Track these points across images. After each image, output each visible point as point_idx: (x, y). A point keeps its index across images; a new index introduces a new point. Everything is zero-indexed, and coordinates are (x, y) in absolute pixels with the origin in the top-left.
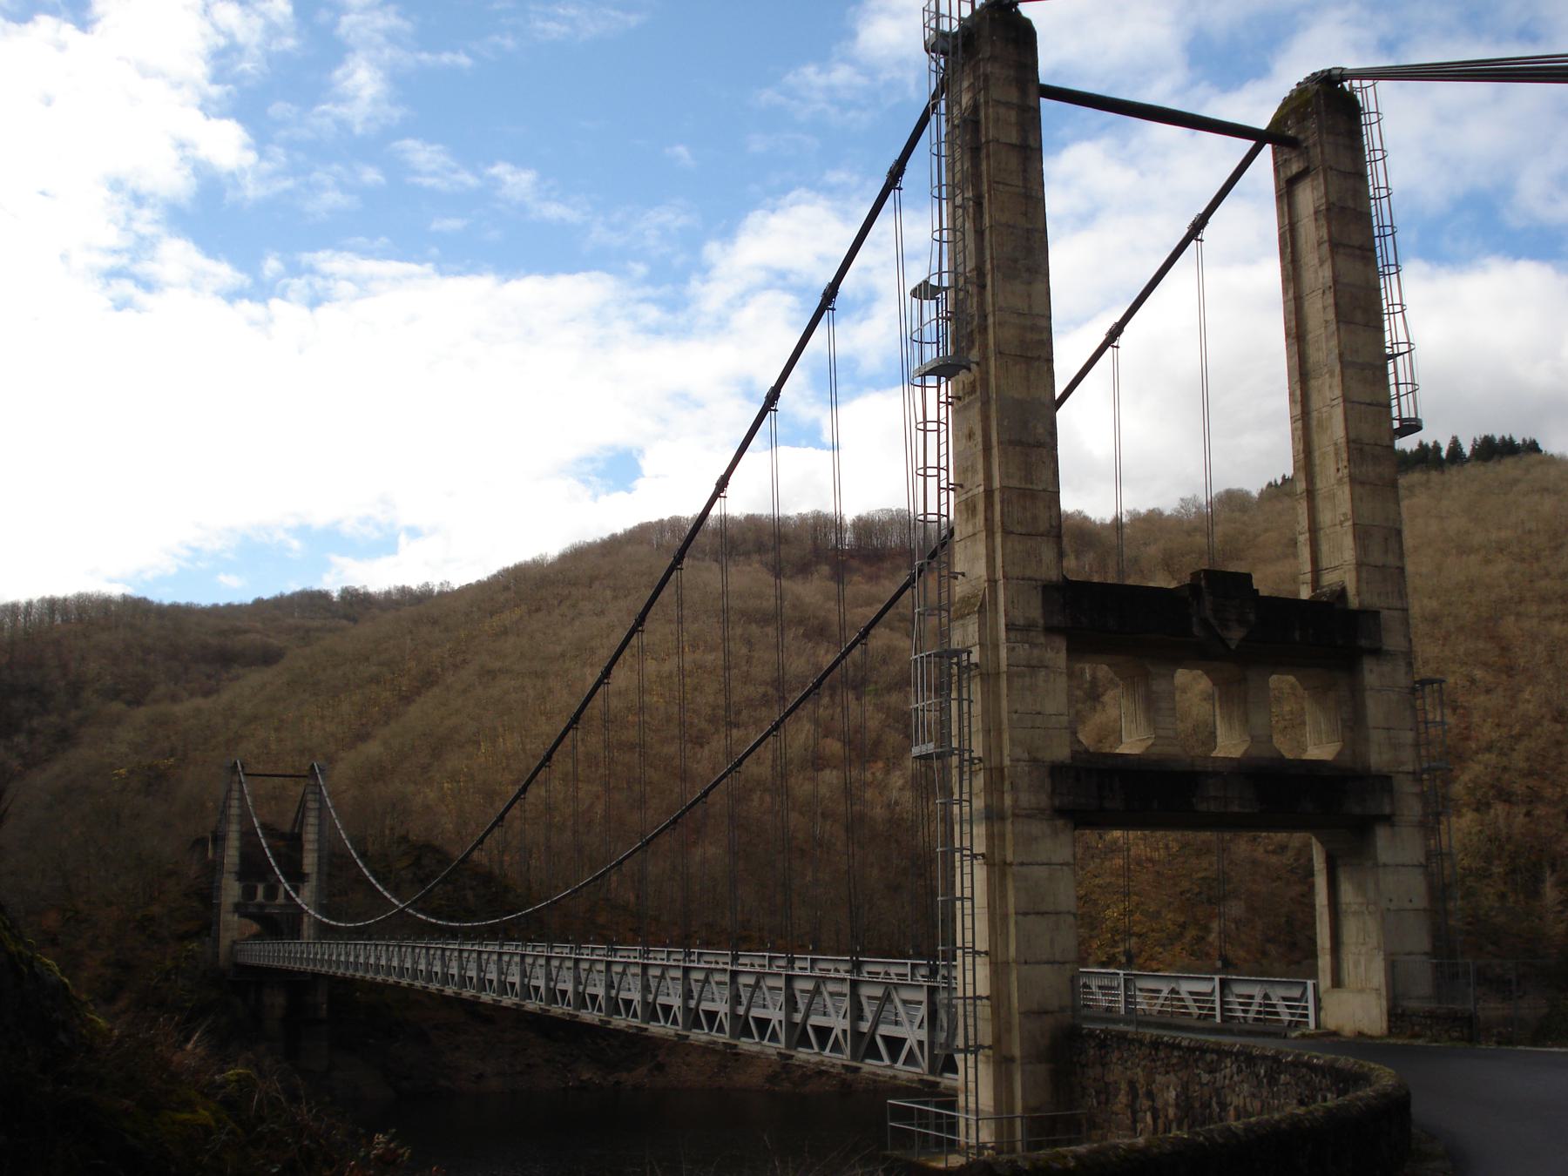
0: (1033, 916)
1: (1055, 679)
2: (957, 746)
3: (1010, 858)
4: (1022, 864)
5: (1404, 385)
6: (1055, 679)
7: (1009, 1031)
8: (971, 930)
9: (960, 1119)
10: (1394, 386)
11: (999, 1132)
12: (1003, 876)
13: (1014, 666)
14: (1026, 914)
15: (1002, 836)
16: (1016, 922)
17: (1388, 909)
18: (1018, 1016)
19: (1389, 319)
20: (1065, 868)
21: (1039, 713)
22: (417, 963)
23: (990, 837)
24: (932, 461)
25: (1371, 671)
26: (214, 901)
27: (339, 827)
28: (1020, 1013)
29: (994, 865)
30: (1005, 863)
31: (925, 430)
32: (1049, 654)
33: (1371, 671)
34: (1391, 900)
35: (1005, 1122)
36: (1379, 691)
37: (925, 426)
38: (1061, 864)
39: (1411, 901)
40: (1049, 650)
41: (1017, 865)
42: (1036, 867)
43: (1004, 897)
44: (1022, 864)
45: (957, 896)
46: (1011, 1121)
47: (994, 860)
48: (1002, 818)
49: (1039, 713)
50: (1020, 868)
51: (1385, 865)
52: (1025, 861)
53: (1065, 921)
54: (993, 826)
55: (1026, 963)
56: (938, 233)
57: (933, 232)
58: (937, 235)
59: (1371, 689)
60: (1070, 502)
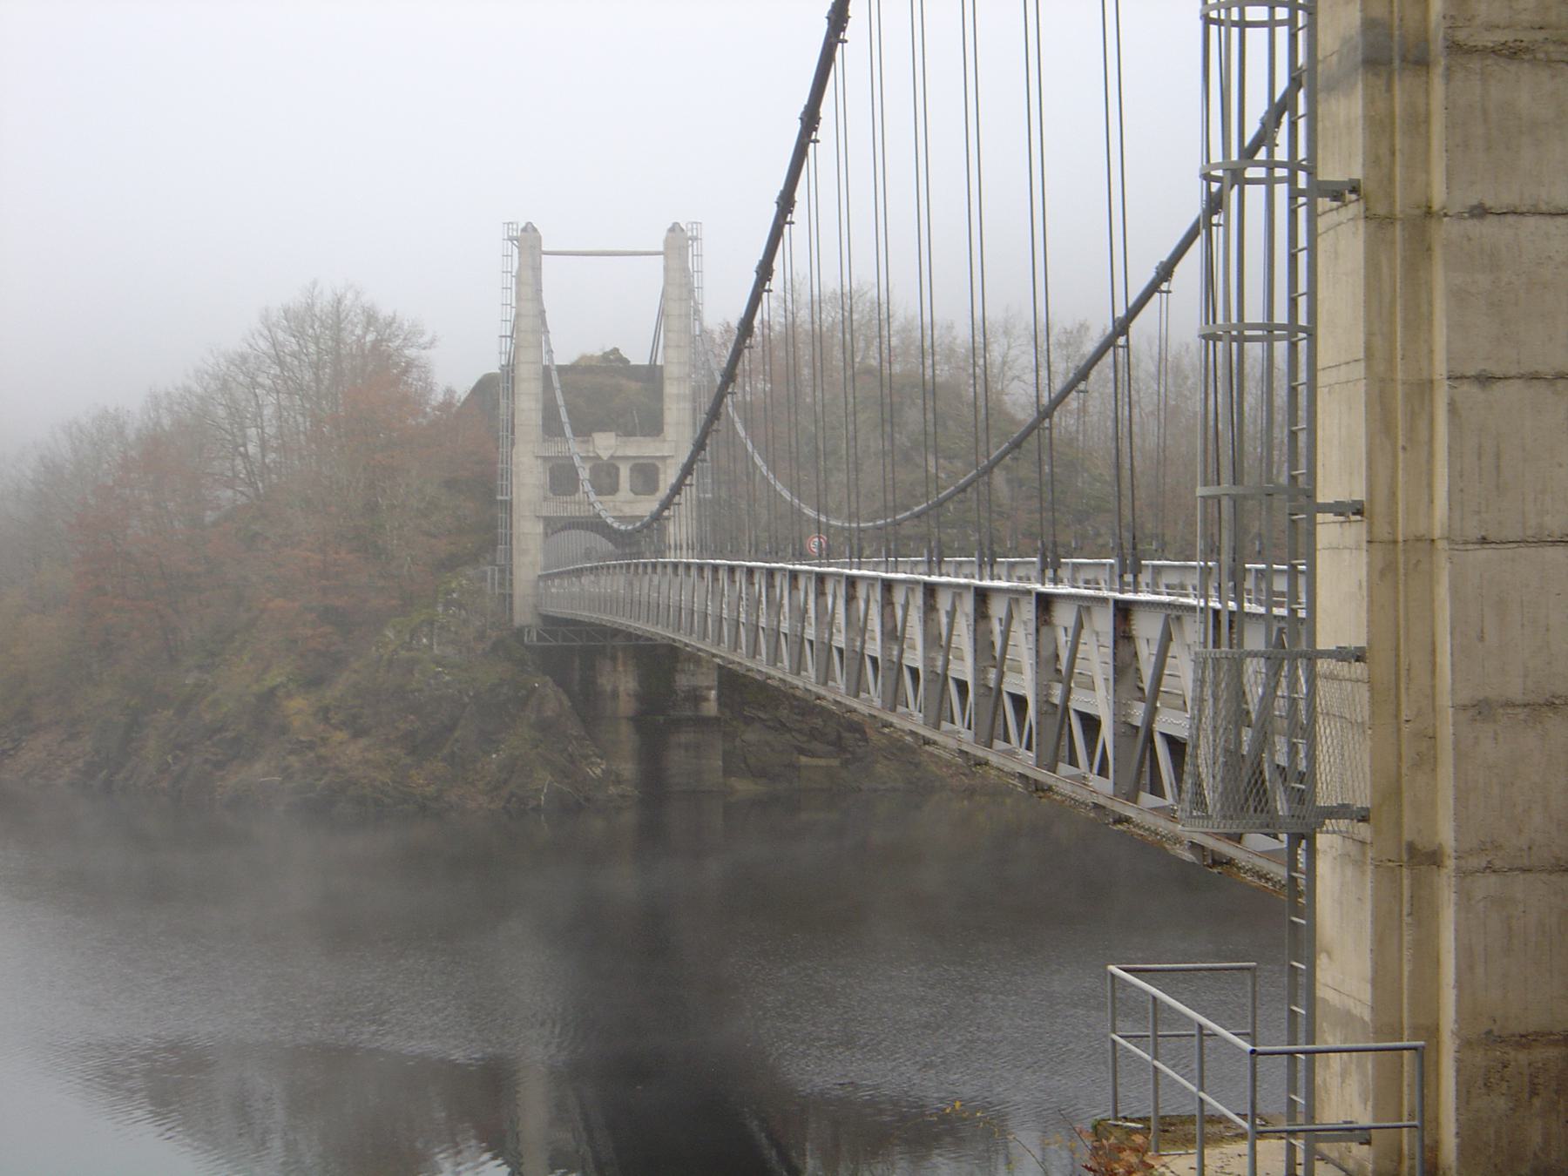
0: (1518, 383)
2: (1285, 159)
3: (1438, 198)
4: (1480, 212)
7: (1427, 761)
8: (1320, 365)
9: (1300, 745)
11: (1385, 1092)
12: (1420, 250)
14: (1485, 380)
15: (1419, 123)
16: (1452, 408)
18: (1450, 711)
22: (1066, 679)
23: (1379, 126)
26: (499, 498)
27: (840, 524)
28: (1460, 708)
29: (1390, 219)
30: (1428, 212)
35: (1225, 503)
41: (1460, 216)
42: (1531, 221)
43: (1419, 321)
44: (1480, 212)
45: (1248, 9)
46: (1425, 1058)
47: (1392, 204)
48: (1421, 63)
50: (1475, 227)
52: (1489, 203)
54: (1389, 88)
55: (1484, 541)
60: (1318, 648)
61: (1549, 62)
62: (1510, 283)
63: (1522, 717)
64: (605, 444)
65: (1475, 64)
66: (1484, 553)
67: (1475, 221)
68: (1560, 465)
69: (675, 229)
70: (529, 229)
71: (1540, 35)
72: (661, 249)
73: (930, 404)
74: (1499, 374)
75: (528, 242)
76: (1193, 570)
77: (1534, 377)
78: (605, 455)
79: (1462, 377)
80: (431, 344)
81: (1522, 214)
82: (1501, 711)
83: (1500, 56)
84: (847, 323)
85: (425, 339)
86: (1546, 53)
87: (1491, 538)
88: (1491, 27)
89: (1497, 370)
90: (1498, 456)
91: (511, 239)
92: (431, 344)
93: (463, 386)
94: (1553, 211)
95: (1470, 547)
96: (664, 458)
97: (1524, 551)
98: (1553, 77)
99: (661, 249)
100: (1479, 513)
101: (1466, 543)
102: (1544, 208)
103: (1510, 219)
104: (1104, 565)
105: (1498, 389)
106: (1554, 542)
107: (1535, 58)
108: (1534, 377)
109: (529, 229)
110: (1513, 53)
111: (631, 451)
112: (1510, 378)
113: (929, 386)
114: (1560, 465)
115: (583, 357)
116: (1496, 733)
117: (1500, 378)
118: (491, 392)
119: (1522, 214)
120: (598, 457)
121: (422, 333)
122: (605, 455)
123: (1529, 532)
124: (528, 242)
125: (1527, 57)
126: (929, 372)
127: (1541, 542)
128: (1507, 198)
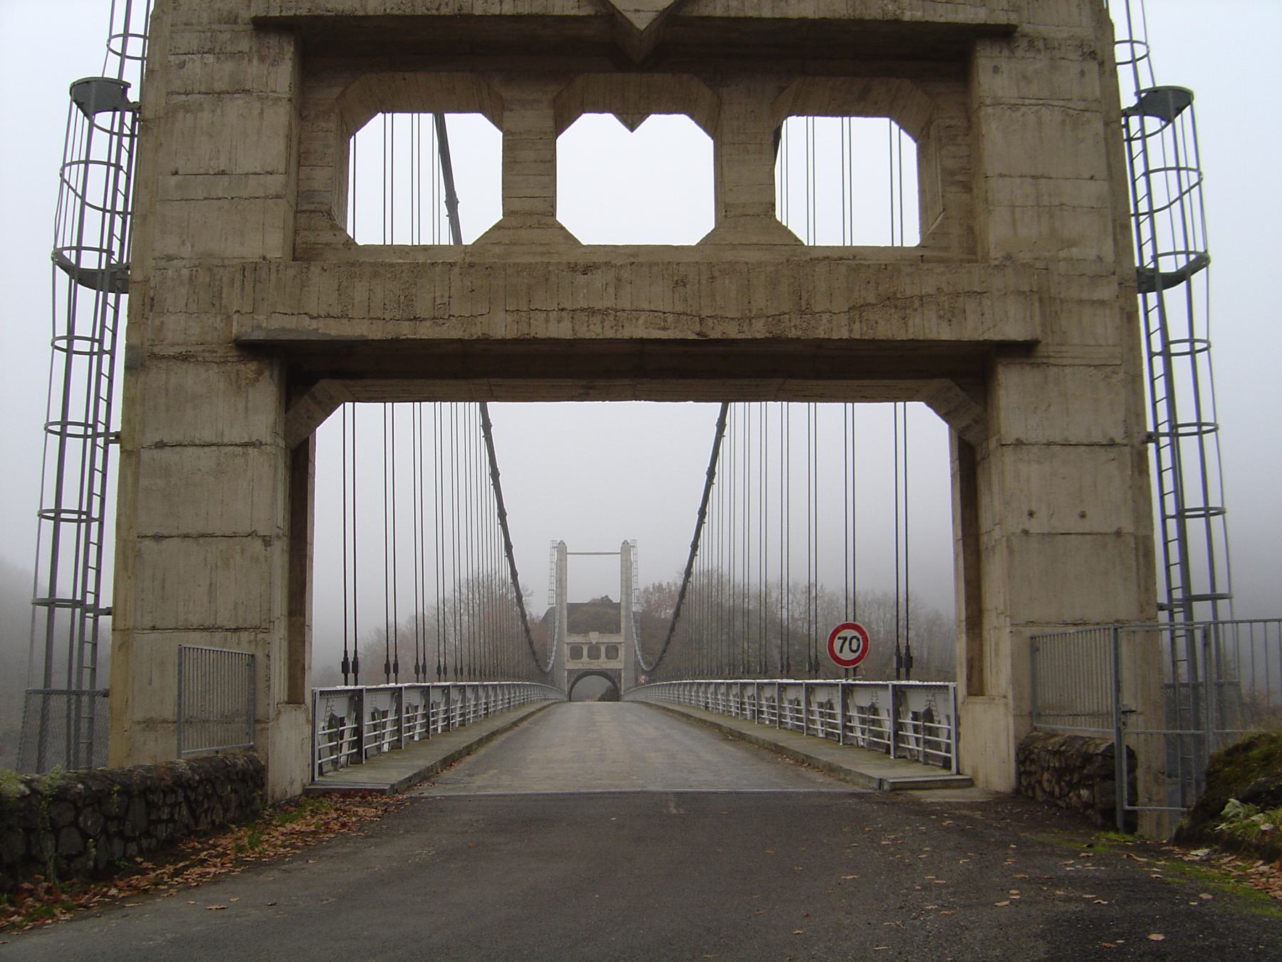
1: (262, 112)
5: (1177, 250)
6: (262, 112)
10: (1143, 178)
13: (179, 94)
17: (1026, 532)
19: (1170, 591)
20: (250, 450)
21: (223, 173)
24: (76, 413)
25: (996, 70)
31: (69, 352)
32: (254, 69)
33: (996, 70)
34: (1031, 514)
36: (1014, 107)
37: (70, 344)
38: (245, 445)
39: (1083, 516)
40: (255, 62)
41: (150, 447)
42: (190, 449)
49: (223, 173)
51: (1019, 443)
53: (243, 551)
55: (154, 628)
56: (121, 39)
57: (111, 37)
58: (117, 44)
59: (997, 103)
61: (205, 362)
62: (175, 484)
63: (172, 728)
64: (594, 637)
65: (163, 365)
66: (155, 635)
67: (159, 451)
68: (199, 586)
69: (625, 543)
70: (562, 543)
71: (201, 348)
72: (619, 551)
73: (746, 619)
74: (166, 535)
75: (561, 549)
76: (835, 688)
77: (186, 536)
78: (594, 642)
79: (146, 537)
80: (531, 594)
81: (185, 446)
82: (160, 725)
83: (178, 360)
84: (710, 584)
85: (529, 592)
86: (203, 358)
87: (157, 626)
88: (173, 345)
89: (165, 533)
90: (164, 580)
91: (554, 548)
92: (531, 594)
93: (542, 614)
94: (203, 443)
95: (146, 632)
96: (620, 643)
97: (176, 634)
98: (207, 370)
99: (619, 551)
100: (151, 612)
101: (143, 629)
102: (197, 442)
103: (178, 449)
104: (774, 684)
105: (165, 542)
106: (195, 630)
107: (197, 361)
108: (186, 536)
109: (562, 543)
110: (184, 358)
111: (606, 640)
112: (212, 536)
113: (746, 610)
114: (199, 586)
115: (594, 600)
116: (156, 737)
117: (167, 537)
118: (550, 613)
119: (185, 446)
120: (591, 643)
121: (527, 590)
122: (594, 642)
123: (180, 623)
124: (561, 549)
125: (192, 360)
126: (746, 605)
127: (187, 629)
128: (178, 437)
